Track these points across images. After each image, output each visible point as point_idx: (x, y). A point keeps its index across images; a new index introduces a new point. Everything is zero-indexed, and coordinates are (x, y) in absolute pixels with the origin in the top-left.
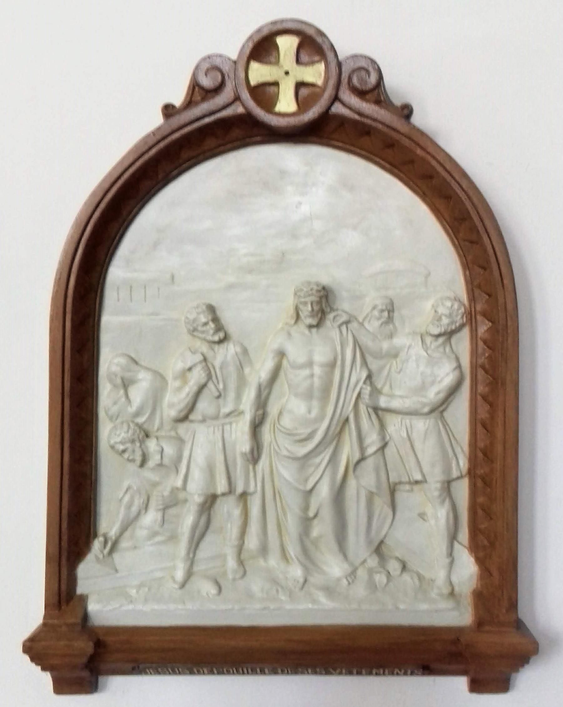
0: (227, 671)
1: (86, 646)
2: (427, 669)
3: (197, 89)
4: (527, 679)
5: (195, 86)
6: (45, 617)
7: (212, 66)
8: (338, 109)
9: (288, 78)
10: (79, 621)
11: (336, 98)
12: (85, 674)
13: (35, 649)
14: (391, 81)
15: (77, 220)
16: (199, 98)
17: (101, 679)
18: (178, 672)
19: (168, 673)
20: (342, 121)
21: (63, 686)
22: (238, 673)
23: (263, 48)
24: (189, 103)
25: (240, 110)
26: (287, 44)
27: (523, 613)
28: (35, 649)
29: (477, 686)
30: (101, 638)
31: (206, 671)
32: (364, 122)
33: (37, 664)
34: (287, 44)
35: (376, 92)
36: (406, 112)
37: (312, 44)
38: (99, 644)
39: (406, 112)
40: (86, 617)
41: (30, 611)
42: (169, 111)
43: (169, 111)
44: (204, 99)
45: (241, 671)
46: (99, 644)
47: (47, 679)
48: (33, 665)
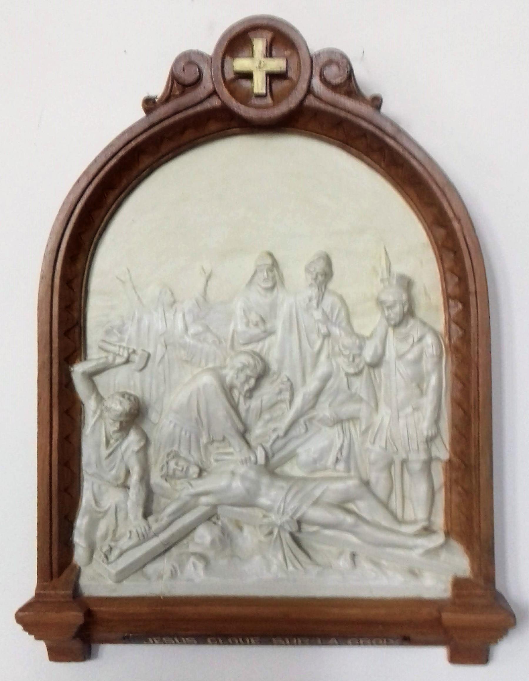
0: (232, 641)
1: (75, 617)
2: (406, 640)
3: (175, 83)
4: (504, 651)
5: (173, 78)
6: (39, 587)
7: (188, 59)
8: (311, 101)
9: (258, 62)
10: (70, 592)
11: (309, 91)
12: (77, 645)
13: (30, 618)
14: (360, 74)
15: (449, 185)
16: (178, 93)
17: (94, 646)
18: (152, 642)
19: (173, 642)
20: (316, 113)
21: (57, 654)
22: (372, 644)
23: (237, 41)
24: (168, 98)
25: (215, 102)
26: (259, 45)
27: (499, 587)
28: (30, 618)
29: (457, 657)
30: (91, 608)
31: (156, 641)
32: (334, 112)
33: (30, 633)
34: (259, 45)
35: (349, 86)
36: (376, 102)
37: (281, 38)
38: (89, 614)
39: (376, 103)
40: (76, 588)
41: (23, 582)
42: (149, 104)
43: (149, 104)
44: (183, 93)
45: (248, 641)
46: (89, 614)
47: (41, 648)
48: (26, 634)
